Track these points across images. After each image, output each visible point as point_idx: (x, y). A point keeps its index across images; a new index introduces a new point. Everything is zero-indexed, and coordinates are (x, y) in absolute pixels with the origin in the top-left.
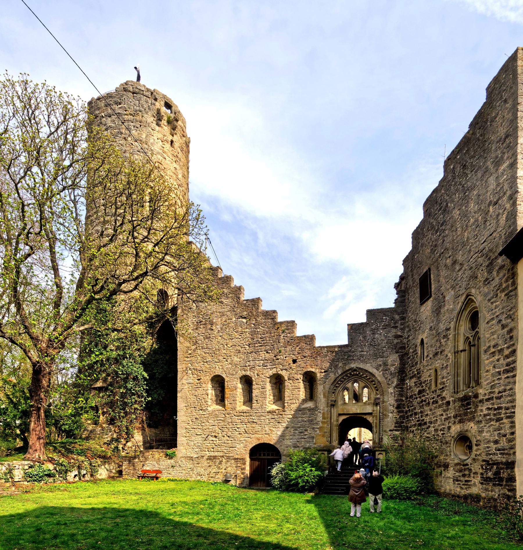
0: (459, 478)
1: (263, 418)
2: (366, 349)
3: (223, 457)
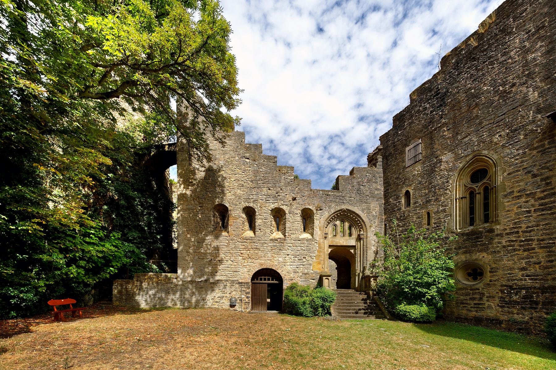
0: (464, 302)
1: (266, 245)
2: (353, 195)
3: (227, 281)
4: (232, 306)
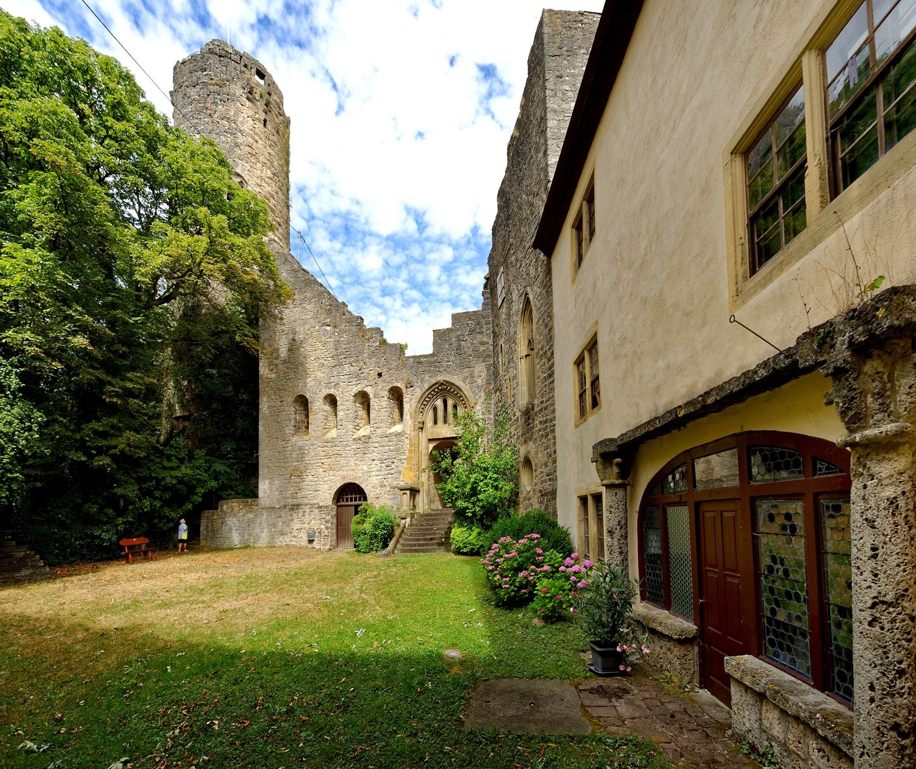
2: (452, 358)
4: (311, 541)
